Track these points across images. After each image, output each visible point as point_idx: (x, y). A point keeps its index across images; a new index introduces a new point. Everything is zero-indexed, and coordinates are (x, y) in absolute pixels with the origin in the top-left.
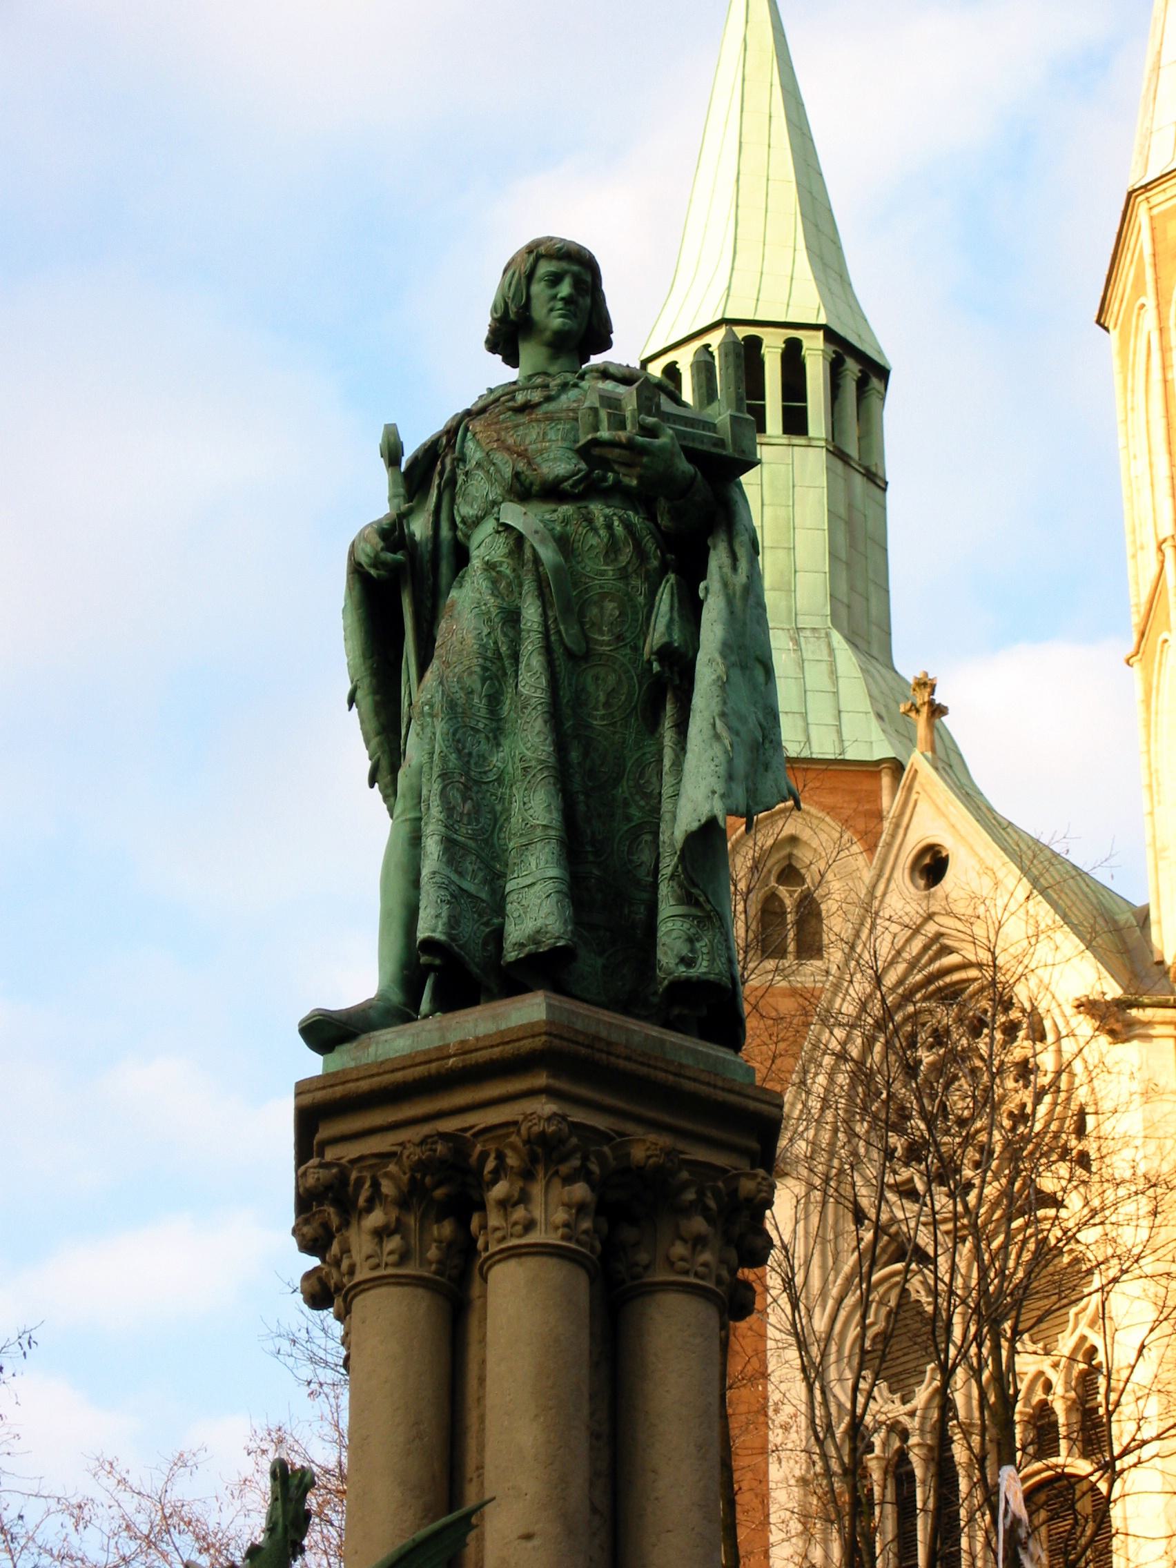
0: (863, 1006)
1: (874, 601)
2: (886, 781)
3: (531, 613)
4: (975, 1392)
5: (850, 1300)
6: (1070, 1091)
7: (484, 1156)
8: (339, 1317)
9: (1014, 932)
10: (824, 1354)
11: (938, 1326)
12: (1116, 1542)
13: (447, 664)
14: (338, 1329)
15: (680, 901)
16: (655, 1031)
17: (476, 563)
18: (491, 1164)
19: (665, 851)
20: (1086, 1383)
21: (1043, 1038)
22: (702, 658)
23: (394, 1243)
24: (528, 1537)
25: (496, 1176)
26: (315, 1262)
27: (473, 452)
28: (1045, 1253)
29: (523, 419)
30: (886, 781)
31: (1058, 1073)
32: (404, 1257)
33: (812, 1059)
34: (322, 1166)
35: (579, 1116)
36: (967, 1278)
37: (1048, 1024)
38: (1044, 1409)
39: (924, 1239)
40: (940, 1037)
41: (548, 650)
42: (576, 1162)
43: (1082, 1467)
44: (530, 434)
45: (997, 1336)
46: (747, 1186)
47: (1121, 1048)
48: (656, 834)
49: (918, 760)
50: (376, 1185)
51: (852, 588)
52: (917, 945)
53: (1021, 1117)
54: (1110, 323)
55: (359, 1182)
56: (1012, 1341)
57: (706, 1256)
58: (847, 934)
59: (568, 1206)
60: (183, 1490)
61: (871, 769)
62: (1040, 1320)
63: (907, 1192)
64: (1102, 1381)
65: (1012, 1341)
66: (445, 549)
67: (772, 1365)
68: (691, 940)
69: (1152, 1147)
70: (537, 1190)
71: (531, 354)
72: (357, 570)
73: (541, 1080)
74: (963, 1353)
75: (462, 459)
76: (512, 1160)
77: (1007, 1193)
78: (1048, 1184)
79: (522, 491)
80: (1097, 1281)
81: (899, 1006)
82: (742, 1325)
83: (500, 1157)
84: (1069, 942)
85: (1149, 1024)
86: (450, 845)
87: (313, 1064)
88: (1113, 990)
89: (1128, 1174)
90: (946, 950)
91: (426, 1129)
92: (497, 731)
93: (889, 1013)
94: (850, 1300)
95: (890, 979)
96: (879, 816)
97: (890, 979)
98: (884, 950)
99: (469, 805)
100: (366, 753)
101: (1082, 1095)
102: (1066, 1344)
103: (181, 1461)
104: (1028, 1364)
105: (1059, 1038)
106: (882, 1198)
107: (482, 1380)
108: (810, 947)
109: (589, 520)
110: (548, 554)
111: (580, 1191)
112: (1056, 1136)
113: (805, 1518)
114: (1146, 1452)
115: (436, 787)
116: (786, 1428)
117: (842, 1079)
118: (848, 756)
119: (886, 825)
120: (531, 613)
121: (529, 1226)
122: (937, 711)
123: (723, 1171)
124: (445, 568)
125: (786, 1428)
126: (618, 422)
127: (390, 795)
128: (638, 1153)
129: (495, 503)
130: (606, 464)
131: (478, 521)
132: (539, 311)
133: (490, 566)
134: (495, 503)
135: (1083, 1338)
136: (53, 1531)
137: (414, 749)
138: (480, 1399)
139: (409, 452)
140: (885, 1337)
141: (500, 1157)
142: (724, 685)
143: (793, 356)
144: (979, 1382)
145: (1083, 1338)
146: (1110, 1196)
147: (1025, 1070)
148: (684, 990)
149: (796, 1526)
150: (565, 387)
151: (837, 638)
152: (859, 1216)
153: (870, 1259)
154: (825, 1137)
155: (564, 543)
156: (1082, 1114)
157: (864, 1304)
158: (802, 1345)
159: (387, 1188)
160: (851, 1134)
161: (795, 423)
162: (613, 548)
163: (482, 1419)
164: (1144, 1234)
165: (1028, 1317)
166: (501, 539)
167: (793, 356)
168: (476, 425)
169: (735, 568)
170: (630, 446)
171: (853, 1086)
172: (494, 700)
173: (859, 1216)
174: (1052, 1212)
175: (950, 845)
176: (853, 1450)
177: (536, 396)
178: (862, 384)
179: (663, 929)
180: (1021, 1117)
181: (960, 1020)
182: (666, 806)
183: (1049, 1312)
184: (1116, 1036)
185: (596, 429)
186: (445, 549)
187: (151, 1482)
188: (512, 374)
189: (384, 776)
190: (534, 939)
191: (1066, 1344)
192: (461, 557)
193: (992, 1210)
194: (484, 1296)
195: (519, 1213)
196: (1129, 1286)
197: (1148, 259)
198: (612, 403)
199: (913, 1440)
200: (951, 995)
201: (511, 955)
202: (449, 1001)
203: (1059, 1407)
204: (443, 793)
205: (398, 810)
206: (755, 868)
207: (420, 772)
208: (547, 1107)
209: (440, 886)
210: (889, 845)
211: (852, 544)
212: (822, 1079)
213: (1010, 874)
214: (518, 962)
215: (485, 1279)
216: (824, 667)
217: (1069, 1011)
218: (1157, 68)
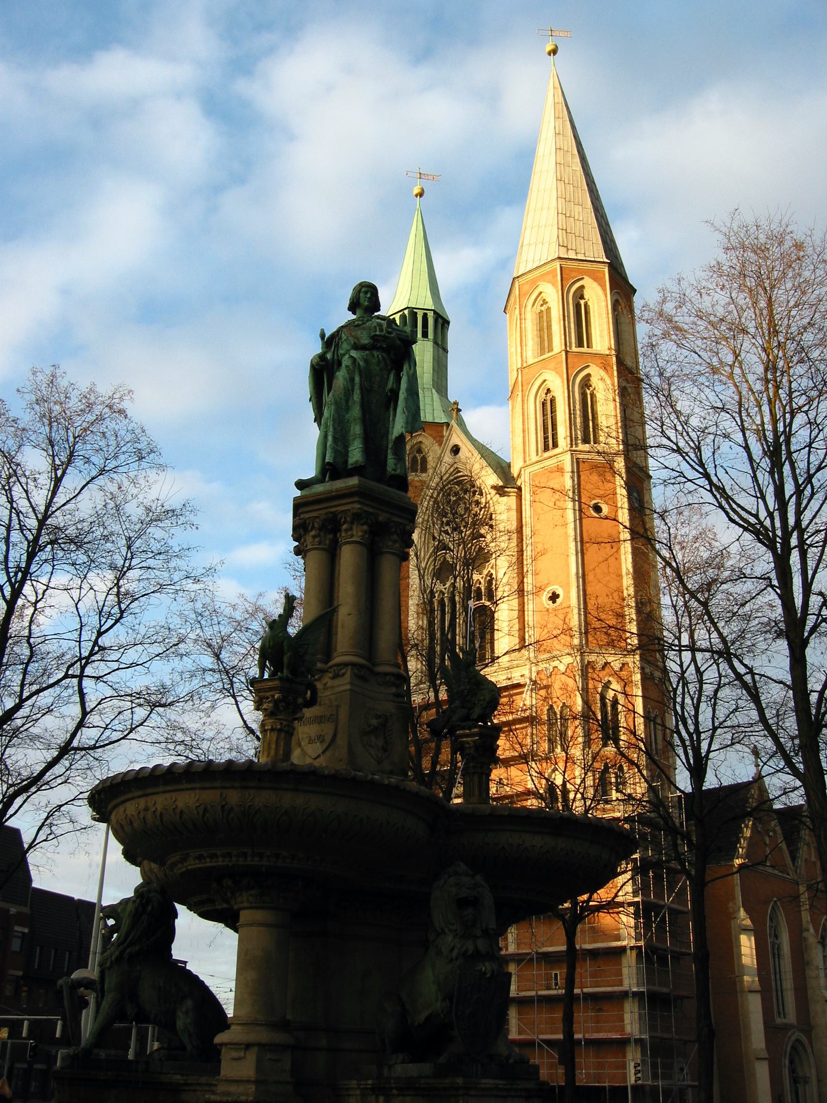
0: (437, 485)
1: (444, 382)
2: (445, 428)
3: (357, 379)
4: (462, 583)
5: (431, 559)
6: (489, 507)
7: (341, 518)
8: (303, 558)
9: (477, 467)
10: (424, 572)
11: (453, 567)
12: (496, 622)
13: (335, 391)
14: (302, 561)
15: (393, 455)
16: (386, 488)
17: (343, 365)
18: (343, 520)
19: (390, 442)
20: (490, 583)
21: (482, 495)
22: (401, 392)
23: (317, 539)
24: (349, 614)
25: (344, 523)
26: (297, 543)
27: (344, 337)
28: (481, 549)
29: (357, 328)
30: (445, 428)
31: (486, 503)
32: (320, 543)
33: (424, 497)
34: (300, 519)
35: (366, 509)
36: (461, 554)
37: (483, 491)
38: (479, 588)
39: (450, 545)
40: (456, 494)
41: (361, 389)
42: (365, 520)
43: (488, 603)
44: (359, 333)
45: (468, 569)
46: (408, 528)
47: (502, 498)
48: (388, 437)
49: (453, 423)
50: (313, 524)
51: (438, 378)
52: (452, 470)
53: (476, 515)
54: (507, 312)
55: (309, 523)
56: (472, 571)
57: (397, 545)
58: (434, 466)
59: (362, 531)
60: (261, 602)
61: (441, 425)
62: (478, 566)
63: (446, 532)
64: (494, 582)
65: (472, 571)
66: (335, 361)
67: (411, 575)
68: (396, 465)
69: (509, 523)
70: (354, 527)
71: (358, 312)
72: (313, 367)
73: (356, 499)
74: (460, 572)
75: (341, 338)
76: (348, 519)
77: (472, 533)
78: (482, 531)
79: (356, 347)
80: (494, 556)
81: (447, 485)
82: (404, 564)
83: (345, 518)
84: (490, 470)
85: (510, 492)
86: (334, 438)
87: (298, 493)
88: (501, 483)
89: (503, 529)
90: (460, 472)
91: (327, 510)
92: (348, 409)
93: (444, 486)
94: (431, 559)
95: (444, 478)
96: (443, 437)
97: (444, 478)
98: (443, 470)
99: (339, 428)
100: (314, 432)
101: (492, 509)
102: (485, 572)
103: (260, 595)
104: (476, 577)
105: (486, 494)
106: (440, 534)
107: (339, 574)
108: (424, 469)
109: (373, 355)
110: (362, 364)
111: (365, 527)
112: (485, 519)
113: (418, 614)
114: (505, 599)
115: (332, 423)
116: (414, 591)
117: (431, 503)
118: (436, 421)
119: (445, 439)
120: (357, 379)
121: (352, 536)
122: (459, 410)
123: (402, 523)
124: (335, 367)
125: (414, 591)
126: (381, 330)
127: (319, 425)
128: (381, 519)
129: (349, 350)
130: (378, 341)
131: (344, 355)
132: (362, 301)
133: (347, 366)
134: (349, 350)
135: (489, 571)
136: (228, 611)
137: (326, 413)
138: (338, 580)
139: (327, 336)
140: (440, 569)
141: (345, 518)
142: (406, 399)
143: (425, 317)
144: (463, 581)
145: (489, 571)
146: (498, 534)
147: (478, 503)
148: (393, 477)
149: (415, 616)
150: (368, 321)
151: (434, 391)
152: (434, 538)
153: (437, 549)
154: (426, 518)
155: (366, 361)
156: (491, 514)
157: (435, 560)
158: (419, 571)
159: (316, 525)
160: (433, 517)
161: (425, 335)
162: (379, 363)
163: (339, 584)
164: (506, 545)
165: (476, 565)
166: (350, 360)
167: (425, 317)
168: (345, 330)
169: (410, 369)
170: (384, 336)
171: (434, 504)
172: (347, 401)
173: (434, 538)
174: (483, 539)
175: (460, 444)
176: (431, 597)
177: (360, 323)
178: (443, 326)
179: (389, 462)
180: (476, 515)
181: (461, 489)
182: (390, 430)
183: (482, 563)
184: (501, 495)
185: (376, 331)
186: (335, 361)
187: (253, 600)
188: (354, 317)
189: (318, 420)
190: (356, 462)
191: (485, 572)
192: (340, 364)
193: (468, 537)
194: (340, 554)
195: (350, 533)
196: (502, 558)
197: (518, 296)
198: (380, 325)
199: (446, 595)
200: (459, 483)
201: (350, 467)
202: (334, 478)
203: (483, 589)
204: (333, 425)
205: (321, 428)
206: (411, 448)
207: (327, 419)
208: (358, 506)
209: (332, 448)
210: (445, 444)
211: (439, 366)
212: (426, 503)
213: (476, 453)
214: (351, 468)
215: (340, 550)
216: (430, 398)
217: (489, 488)
218: (522, 246)
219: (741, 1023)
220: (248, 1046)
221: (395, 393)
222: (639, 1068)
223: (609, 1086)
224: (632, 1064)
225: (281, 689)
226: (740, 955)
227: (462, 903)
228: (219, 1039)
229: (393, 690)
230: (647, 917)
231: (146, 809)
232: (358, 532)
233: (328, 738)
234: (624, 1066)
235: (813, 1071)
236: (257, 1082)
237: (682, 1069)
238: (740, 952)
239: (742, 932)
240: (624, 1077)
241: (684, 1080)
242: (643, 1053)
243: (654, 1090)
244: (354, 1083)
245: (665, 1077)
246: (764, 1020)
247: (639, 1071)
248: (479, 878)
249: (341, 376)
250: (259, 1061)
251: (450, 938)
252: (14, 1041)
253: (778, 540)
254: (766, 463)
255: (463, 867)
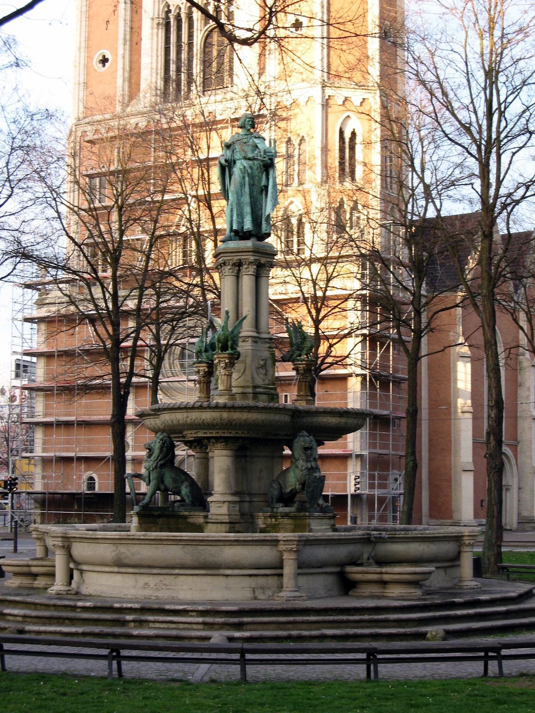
3: (247, 179)
155: (251, 168)
162: (257, 169)
219: (452, 439)
220: (224, 502)
221: (266, 187)
222: (358, 480)
223: (332, 495)
224: (353, 477)
225: (228, 358)
226: (456, 380)
227: (306, 449)
228: (209, 499)
229: (268, 345)
230: (373, 348)
231: (187, 417)
232: (252, 269)
233: (242, 371)
234: (345, 478)
235: (516, 480)
236: (229, 515)
237: (396, 480)
238: (456, 377)
239: (461, 359)
240: (345, 487)
241: (396, 489)
242: (363, 467)
243: (371, 499)
244: (261, 514)
245: (381, 486)
246: (474, 436)
247: (359, 483)
248: (311, 437)
249: (237, 170)
250: (229, 507)
251: (301, 462)
252: (344, 526)
253: (483, 142)
254: (480, 76)
255: (305, 433)
